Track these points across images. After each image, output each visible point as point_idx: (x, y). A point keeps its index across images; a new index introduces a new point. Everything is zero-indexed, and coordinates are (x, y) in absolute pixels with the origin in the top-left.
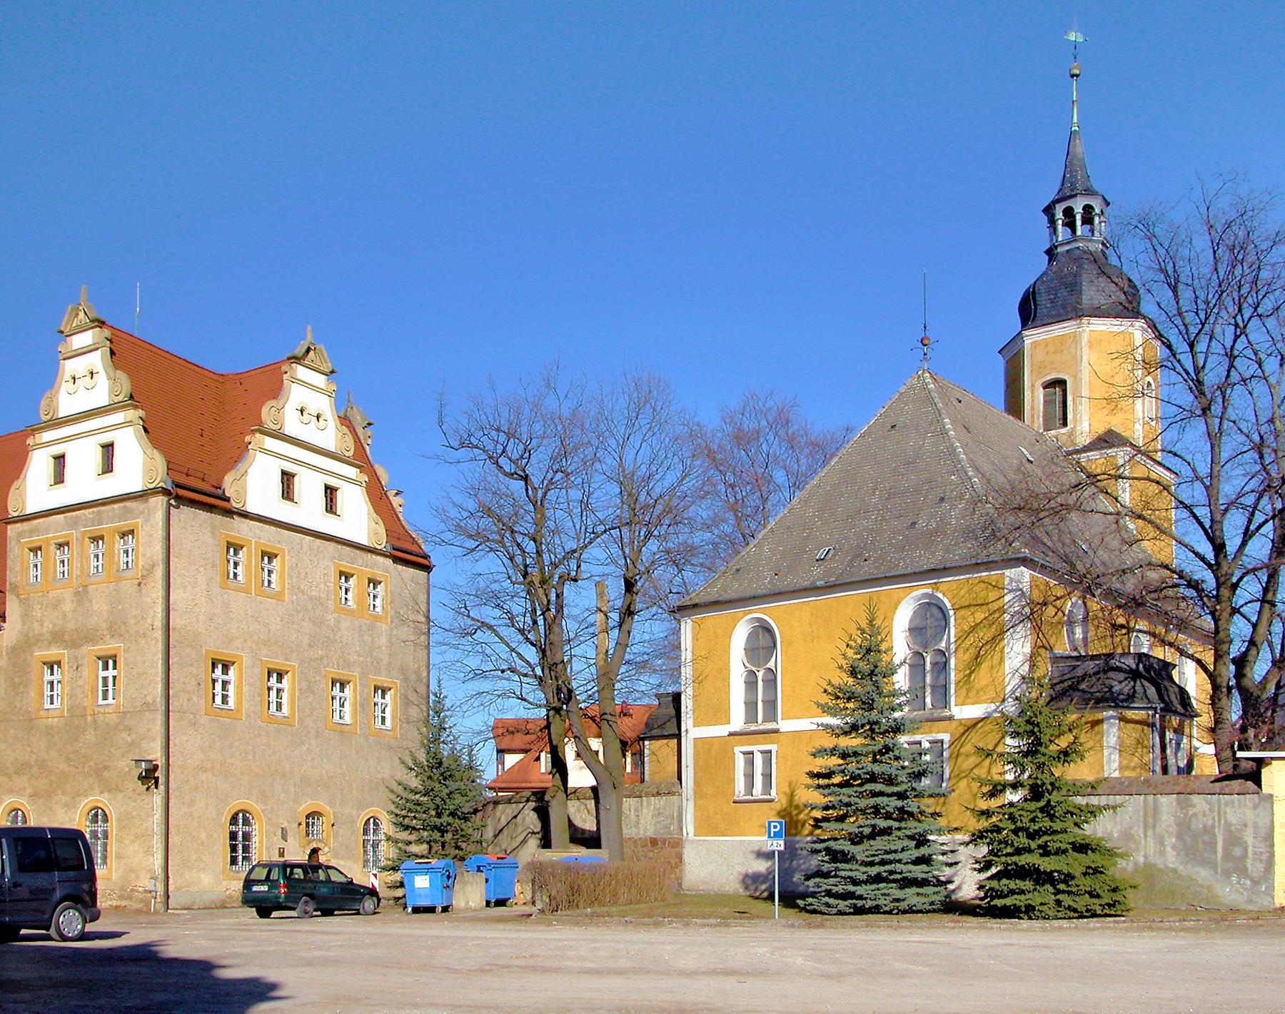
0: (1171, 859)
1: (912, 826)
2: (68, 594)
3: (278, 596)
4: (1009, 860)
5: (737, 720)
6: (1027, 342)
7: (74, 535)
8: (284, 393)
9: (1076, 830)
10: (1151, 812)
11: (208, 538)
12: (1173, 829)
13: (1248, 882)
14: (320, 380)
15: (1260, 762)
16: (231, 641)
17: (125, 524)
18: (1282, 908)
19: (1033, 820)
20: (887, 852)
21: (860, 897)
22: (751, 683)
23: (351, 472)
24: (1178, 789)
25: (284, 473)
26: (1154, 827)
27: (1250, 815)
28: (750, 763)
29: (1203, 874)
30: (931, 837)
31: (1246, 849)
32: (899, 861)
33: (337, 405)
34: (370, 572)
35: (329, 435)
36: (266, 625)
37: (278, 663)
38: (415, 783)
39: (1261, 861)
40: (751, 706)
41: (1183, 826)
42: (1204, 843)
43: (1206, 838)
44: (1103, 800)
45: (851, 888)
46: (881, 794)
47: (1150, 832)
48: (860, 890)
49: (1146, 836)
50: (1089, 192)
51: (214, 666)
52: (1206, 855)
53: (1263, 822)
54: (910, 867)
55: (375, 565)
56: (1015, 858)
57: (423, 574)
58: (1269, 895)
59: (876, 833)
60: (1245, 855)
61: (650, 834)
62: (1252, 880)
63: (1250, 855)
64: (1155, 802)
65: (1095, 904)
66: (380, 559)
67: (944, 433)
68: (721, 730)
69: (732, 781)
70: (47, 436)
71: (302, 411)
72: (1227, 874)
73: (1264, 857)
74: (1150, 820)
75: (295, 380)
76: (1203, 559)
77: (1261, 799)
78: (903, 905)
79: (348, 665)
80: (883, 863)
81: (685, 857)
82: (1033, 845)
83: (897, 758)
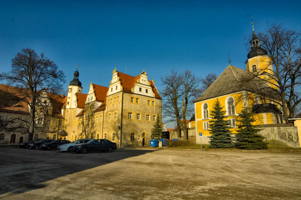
0: (277, 138)
1: (227, 133)
2: (112, 105)
3: (139, 104)
4: (242, 139)
5: (203, 117)
6: (249, 61)
7: (113, 98)
8: (140, 78)
9: (255, 133)
10: (272, 130)
11: (129, 97)
12: (277, 133)
13: (294, 143)
14: (145, 76)
15: (294, 120)
16: (132, 110)
17: (118, 96)
18: (300, 148)
19: (246, 132)
20: (222, 138)
21: (217, 145)
22: (205, 112)
23: (150, 87)
24: (277, 126)
25: (146, 90)
26: (273, 133)
27: (292, 130)
28: (205, 124)
29: (284, 141)
30: (230, 135)
31: (292, 137)
32: (224, 139)
33: (148, 78)
34: (152, 100)
35: (147, 83)
36: (137, 108)
37: (139, 113)
38: (154, 128)
39: (296, 139)
40: (205, 116)
41: (279, 133)
42: (284, 136)
43: (284, 135)
44: (262, 128)
45: (216, 144)
46: (220, 128)
47: (273, 134)
48: (217, 144)
49: (272, 134)
50: (257, 39)
51: (129, 114)
52: (284, 138)
53: (295, 131)
54: (226, 140)
55: (153, 99)
56: (243, 139)
57: (161, 100)
58: (299, 145)
59: (220, 134)
60: (292, 137)
61: (192, 135)
62: (295, 142)
63: (294, 138)
64: (273, 128)
65: (260, 147)
66: (154, 99)
67: (233, 73)
68: (201, 120)
69: (202, 127)
70: (111, 85)
71: (143, 80)
72: (289, 141)
73: (297, 138)
74: (273, 132)
75: (141, 76)
76: (277, 86)
77: (294, 127)
78: (225, 147)
79: (149, 113)
80: (221, 139)
81: (196, 139)
82: (246, 136)
83: (222, 122)
